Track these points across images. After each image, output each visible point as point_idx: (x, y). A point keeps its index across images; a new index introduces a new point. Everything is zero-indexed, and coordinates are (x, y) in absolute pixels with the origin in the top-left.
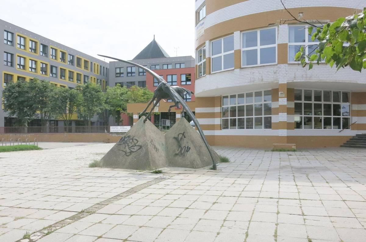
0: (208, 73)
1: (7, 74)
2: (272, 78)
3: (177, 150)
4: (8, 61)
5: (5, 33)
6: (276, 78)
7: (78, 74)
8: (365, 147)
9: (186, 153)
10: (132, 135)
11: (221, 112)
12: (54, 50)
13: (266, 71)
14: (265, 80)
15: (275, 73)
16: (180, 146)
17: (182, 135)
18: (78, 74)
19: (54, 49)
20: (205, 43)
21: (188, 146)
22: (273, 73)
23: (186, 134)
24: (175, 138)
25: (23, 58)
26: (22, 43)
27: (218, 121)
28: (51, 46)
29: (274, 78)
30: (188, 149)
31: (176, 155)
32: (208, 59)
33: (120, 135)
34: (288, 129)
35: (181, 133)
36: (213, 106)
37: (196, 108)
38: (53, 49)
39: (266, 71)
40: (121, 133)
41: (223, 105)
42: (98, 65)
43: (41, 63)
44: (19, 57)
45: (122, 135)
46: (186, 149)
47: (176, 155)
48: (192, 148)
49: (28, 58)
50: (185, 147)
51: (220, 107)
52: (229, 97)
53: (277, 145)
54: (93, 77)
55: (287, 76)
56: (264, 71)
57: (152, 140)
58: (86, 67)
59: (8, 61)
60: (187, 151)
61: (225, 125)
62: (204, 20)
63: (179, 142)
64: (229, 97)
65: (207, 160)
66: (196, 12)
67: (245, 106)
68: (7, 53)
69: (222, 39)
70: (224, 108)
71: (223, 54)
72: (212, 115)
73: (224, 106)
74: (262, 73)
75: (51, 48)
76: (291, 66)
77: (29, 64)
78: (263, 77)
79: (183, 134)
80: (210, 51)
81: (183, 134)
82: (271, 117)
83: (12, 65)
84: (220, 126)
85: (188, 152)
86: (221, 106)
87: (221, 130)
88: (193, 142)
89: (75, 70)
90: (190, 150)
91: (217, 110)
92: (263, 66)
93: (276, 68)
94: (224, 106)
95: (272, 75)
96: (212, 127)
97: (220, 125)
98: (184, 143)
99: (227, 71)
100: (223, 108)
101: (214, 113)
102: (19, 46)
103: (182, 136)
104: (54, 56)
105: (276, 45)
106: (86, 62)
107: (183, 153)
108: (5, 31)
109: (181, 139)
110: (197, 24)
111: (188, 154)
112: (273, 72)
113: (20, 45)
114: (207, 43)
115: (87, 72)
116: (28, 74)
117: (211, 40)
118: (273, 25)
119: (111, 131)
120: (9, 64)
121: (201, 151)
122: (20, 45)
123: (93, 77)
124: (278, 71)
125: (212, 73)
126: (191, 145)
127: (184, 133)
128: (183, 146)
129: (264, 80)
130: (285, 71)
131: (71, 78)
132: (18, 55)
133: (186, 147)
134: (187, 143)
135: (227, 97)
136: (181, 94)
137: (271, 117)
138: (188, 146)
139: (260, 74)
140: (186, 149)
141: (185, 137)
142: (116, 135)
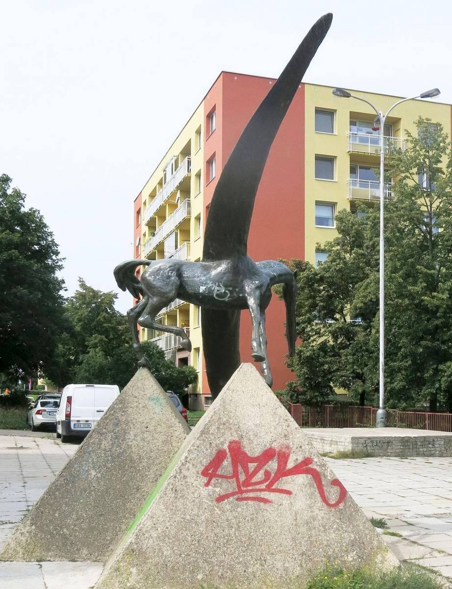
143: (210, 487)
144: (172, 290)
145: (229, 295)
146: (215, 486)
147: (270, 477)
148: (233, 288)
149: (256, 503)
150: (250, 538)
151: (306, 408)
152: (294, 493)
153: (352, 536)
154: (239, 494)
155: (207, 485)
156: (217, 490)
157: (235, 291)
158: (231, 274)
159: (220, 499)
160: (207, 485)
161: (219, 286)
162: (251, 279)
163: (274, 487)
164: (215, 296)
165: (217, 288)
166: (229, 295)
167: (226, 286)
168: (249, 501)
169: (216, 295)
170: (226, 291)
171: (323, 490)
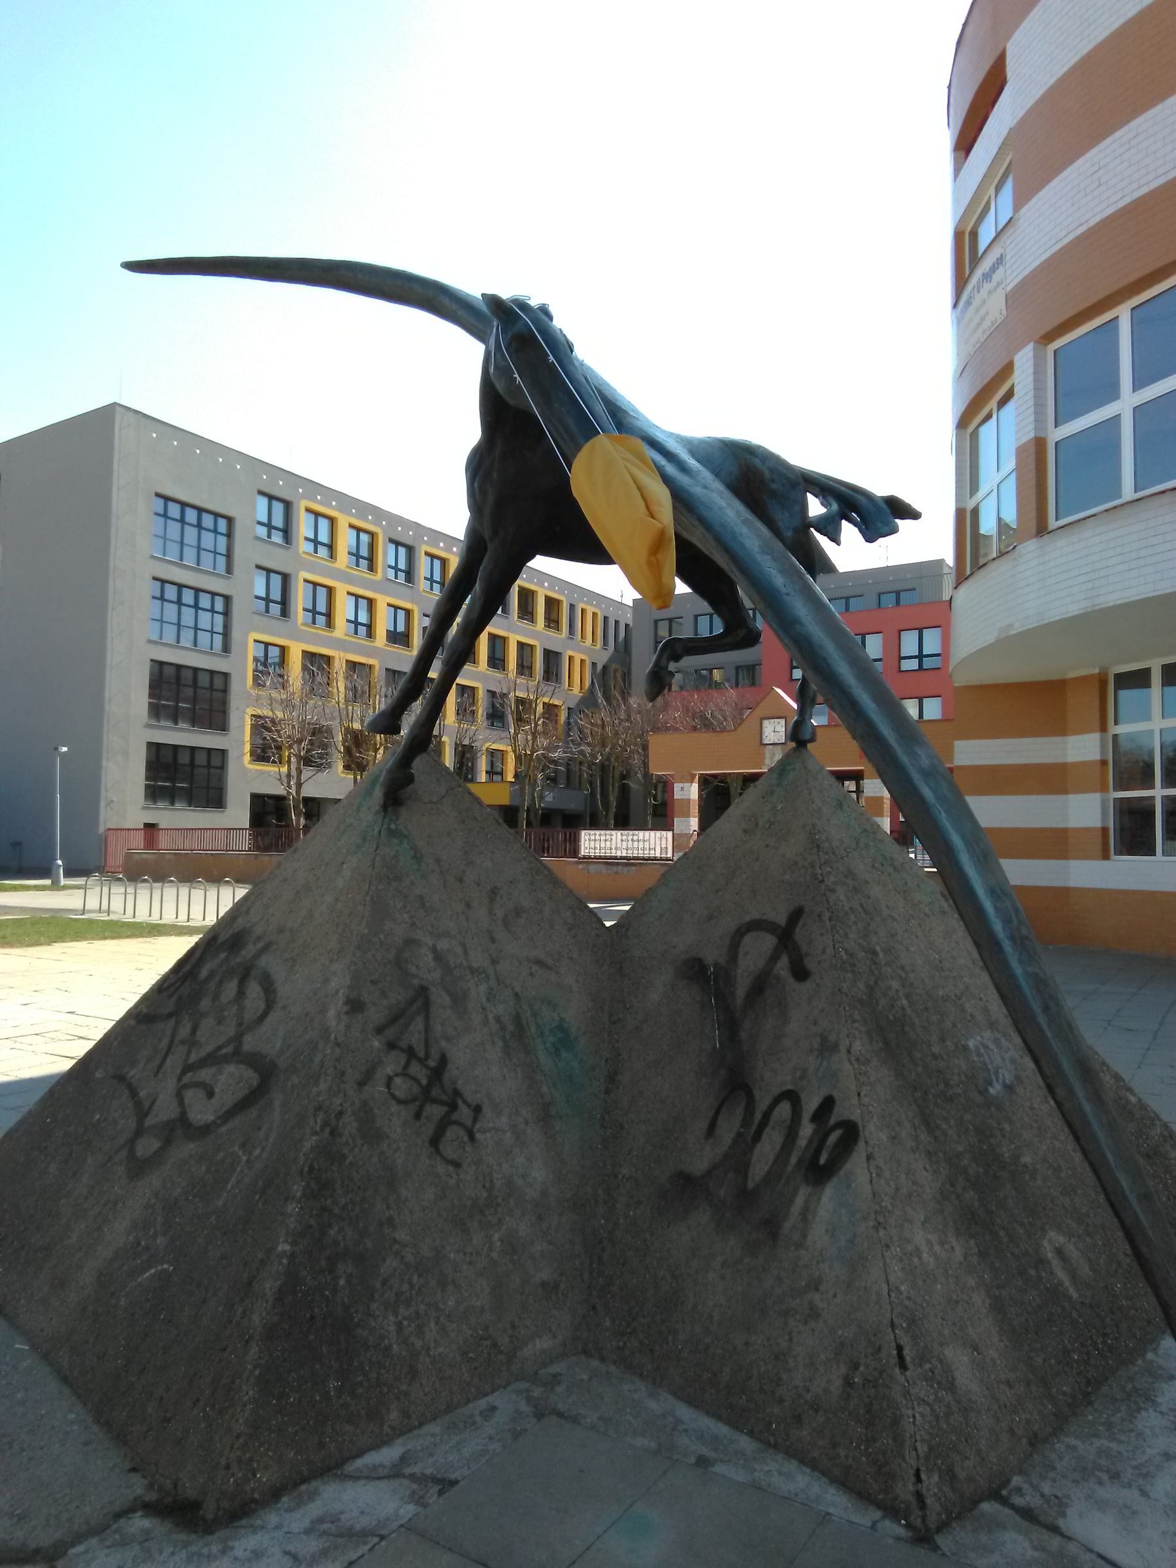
0: (1034, 530)
1: (395, 672)
3: (704, 1125)
4: (318, 609)
5: (262, 503)
7: (521, 645)
9: (804, 1191)
10: (258, 930)
11: (1104, 763)
12: (437, 563)
16: (736, 1083)
17: (768, 942)
18: (521, 645)
19: (438, 558)
20: (1007, 370)
21: (828, 1104)
23: (816, 941)
24: (695, 970)
25: (325, 590)
26: (323, 537)
27: (1086, 811)
28: (425, 548)
30: (834, 1143)
31: (687, 1188)
32: (1032, 450)
33: (620, 868)
35: (772, 916)
36: (1059, 727)
37: (957, 743)
38: (433, 557)
40: (622, 858)
41: (1116, 723)
42: (594, 614)
43: (349, 593)
44: (264, 573)
45: (626, 869)
46: (807, 1130)
47: (687, 1188)
48: (874, 1133)
49: (341, 589)
50: (792, 1096)
51: (1096, 736)
52: (1156, 677)
54: (578, 657)
57: (423, 990)
58: (552, 621)
59: (318, 609)
60: (819, 1172)
61: (1133, 832)
62: (1006, 239)
63: (731, 1026)
64: (1156, 677)
65: (1085, 1271)
66: (958, 236)
68: (269, 571)
69: (1123, 314)
70: (1121, 739)
71: (1126, 403)
72: (1053, 779)
73: (1121, 729)
75: (427, 554)
77: (344, 609)
79: (785, 936)
80: (1044, 405)
81: (785, 936)
83: (285, 613)
84: (1100, 840)
85: (829, 1191)
86: (1103, 728)
87: (1105, 856)
88: (894, 1037)
89: (513, 632)
90: (856, 1165)
91: (1083, 748)
94: (1121, 729)
96: (1055, 843)
97: (1099, 834)
98: (786, 1058)
99: (1163, 492)
100: (1115, 736)
101: (1064, 767)
102: (310, 547)
103: (774, 958)
104: (436, 582)
106: (552, 604)
107: (767, 1179)
108: (261, 493)
109: (761, 984)
110: (960, 281)
111: (826, 1214)
113: (315, 542)
114: (1024, 361)
115: (557, 640)
116: (340, 645)
117: (1049, 337)
119: (583, 852)
120: (276, 609)
121: (1006, 1151)
122: (315, 542)
123: (578, 657)
125: (1053, 524)
126: (867, 1092)
127: (796, 915)
128: (771, 1078)
131: (524, 668)
133: (811, 1104)
134: (827, 1047)
135: (1139, 679)
136: (784, 520)
138: (828, 1104)
140: (807, 1130)
141: (800, 973)
142: (603, 868)
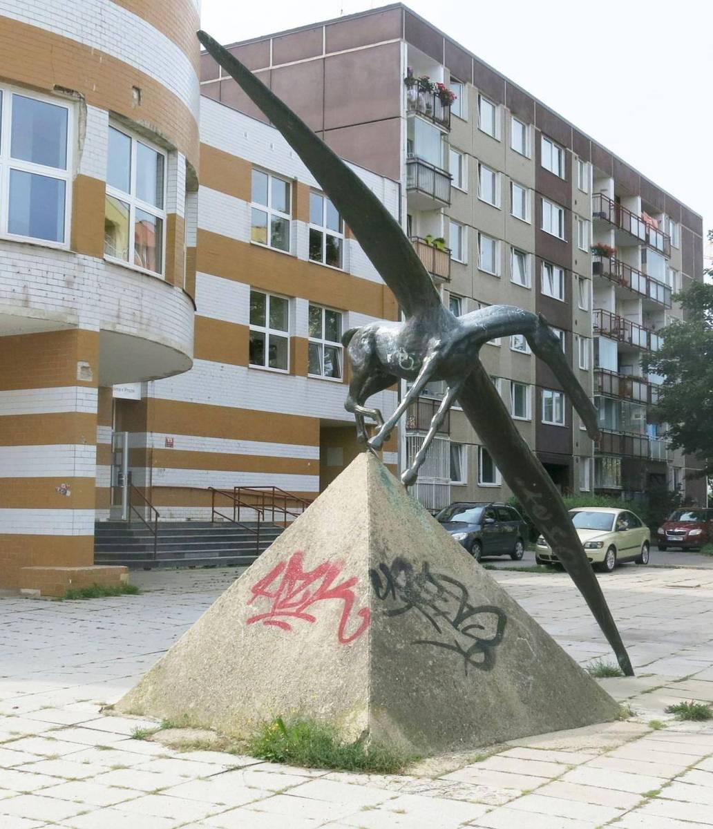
2: (60, 302)
6: (70, 305)
8: (711, 555)
13: (39, 266)
14: (37, 306)
15: (69, 284)
22: (62, 284)
29: (66, 304)
34: (96, 508)
39: (39, 266)
53: (82, 571)
55: (102, 304)
56: (34, 266)
67: (289, 340)
74: (34, 272)
76: (110, 268)
78: (31, 292)
82: (546, 399)
92: (31, 245)
93: (72, 266)
95: (60, 290)
105: (66, 175)
112: (61, 277)
118: (66, 95)
124: (76, 280)
129: (31, 305)
130: (96, 284)
132: (255, 769)
137: (546, 399)
139: (19, 277)
143: (251, 606)
144: (362, 363)
145: (413, 363)
146: (255, 606)
147: (624, 512)
148: (416, 353)
149: (278, 628)
150: (251, 670)
151: (649, 452)
152: (317, 620)
153: (341, 682)
154: (266, 619)
155: (250, 602)
156: (255, 609)
157: (419, 356)
158: (413, 335)
159: (251, 621)
160: (250, 602)
161: (402, 352)
162: (412, 340)
163: (303, 612)
164: (400, 364)
165: (401, 355)
166: (413, 363)
167: (409, 351)
168: (273, 626)
169: (402, 363)
170: (410, 358)
171: (346, 618)
